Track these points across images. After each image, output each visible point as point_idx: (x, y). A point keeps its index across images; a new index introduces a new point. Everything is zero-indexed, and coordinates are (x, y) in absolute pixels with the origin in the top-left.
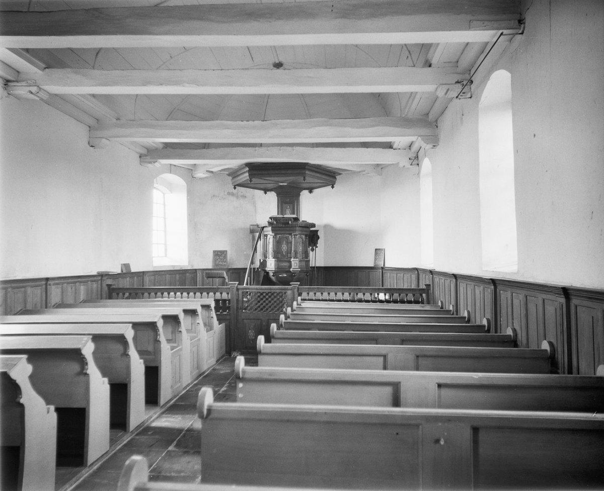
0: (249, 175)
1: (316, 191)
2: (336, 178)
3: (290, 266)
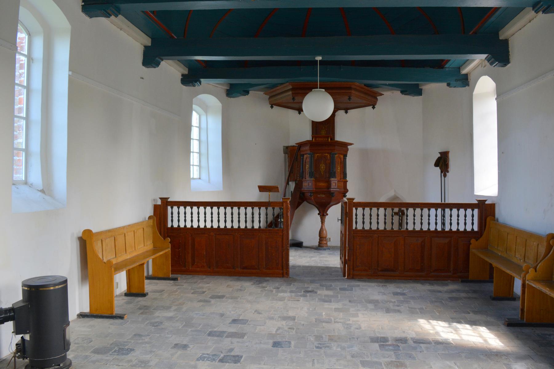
0: (292, 93)
1: (351, 112)
2: (377, 99)
3: (329, 186)
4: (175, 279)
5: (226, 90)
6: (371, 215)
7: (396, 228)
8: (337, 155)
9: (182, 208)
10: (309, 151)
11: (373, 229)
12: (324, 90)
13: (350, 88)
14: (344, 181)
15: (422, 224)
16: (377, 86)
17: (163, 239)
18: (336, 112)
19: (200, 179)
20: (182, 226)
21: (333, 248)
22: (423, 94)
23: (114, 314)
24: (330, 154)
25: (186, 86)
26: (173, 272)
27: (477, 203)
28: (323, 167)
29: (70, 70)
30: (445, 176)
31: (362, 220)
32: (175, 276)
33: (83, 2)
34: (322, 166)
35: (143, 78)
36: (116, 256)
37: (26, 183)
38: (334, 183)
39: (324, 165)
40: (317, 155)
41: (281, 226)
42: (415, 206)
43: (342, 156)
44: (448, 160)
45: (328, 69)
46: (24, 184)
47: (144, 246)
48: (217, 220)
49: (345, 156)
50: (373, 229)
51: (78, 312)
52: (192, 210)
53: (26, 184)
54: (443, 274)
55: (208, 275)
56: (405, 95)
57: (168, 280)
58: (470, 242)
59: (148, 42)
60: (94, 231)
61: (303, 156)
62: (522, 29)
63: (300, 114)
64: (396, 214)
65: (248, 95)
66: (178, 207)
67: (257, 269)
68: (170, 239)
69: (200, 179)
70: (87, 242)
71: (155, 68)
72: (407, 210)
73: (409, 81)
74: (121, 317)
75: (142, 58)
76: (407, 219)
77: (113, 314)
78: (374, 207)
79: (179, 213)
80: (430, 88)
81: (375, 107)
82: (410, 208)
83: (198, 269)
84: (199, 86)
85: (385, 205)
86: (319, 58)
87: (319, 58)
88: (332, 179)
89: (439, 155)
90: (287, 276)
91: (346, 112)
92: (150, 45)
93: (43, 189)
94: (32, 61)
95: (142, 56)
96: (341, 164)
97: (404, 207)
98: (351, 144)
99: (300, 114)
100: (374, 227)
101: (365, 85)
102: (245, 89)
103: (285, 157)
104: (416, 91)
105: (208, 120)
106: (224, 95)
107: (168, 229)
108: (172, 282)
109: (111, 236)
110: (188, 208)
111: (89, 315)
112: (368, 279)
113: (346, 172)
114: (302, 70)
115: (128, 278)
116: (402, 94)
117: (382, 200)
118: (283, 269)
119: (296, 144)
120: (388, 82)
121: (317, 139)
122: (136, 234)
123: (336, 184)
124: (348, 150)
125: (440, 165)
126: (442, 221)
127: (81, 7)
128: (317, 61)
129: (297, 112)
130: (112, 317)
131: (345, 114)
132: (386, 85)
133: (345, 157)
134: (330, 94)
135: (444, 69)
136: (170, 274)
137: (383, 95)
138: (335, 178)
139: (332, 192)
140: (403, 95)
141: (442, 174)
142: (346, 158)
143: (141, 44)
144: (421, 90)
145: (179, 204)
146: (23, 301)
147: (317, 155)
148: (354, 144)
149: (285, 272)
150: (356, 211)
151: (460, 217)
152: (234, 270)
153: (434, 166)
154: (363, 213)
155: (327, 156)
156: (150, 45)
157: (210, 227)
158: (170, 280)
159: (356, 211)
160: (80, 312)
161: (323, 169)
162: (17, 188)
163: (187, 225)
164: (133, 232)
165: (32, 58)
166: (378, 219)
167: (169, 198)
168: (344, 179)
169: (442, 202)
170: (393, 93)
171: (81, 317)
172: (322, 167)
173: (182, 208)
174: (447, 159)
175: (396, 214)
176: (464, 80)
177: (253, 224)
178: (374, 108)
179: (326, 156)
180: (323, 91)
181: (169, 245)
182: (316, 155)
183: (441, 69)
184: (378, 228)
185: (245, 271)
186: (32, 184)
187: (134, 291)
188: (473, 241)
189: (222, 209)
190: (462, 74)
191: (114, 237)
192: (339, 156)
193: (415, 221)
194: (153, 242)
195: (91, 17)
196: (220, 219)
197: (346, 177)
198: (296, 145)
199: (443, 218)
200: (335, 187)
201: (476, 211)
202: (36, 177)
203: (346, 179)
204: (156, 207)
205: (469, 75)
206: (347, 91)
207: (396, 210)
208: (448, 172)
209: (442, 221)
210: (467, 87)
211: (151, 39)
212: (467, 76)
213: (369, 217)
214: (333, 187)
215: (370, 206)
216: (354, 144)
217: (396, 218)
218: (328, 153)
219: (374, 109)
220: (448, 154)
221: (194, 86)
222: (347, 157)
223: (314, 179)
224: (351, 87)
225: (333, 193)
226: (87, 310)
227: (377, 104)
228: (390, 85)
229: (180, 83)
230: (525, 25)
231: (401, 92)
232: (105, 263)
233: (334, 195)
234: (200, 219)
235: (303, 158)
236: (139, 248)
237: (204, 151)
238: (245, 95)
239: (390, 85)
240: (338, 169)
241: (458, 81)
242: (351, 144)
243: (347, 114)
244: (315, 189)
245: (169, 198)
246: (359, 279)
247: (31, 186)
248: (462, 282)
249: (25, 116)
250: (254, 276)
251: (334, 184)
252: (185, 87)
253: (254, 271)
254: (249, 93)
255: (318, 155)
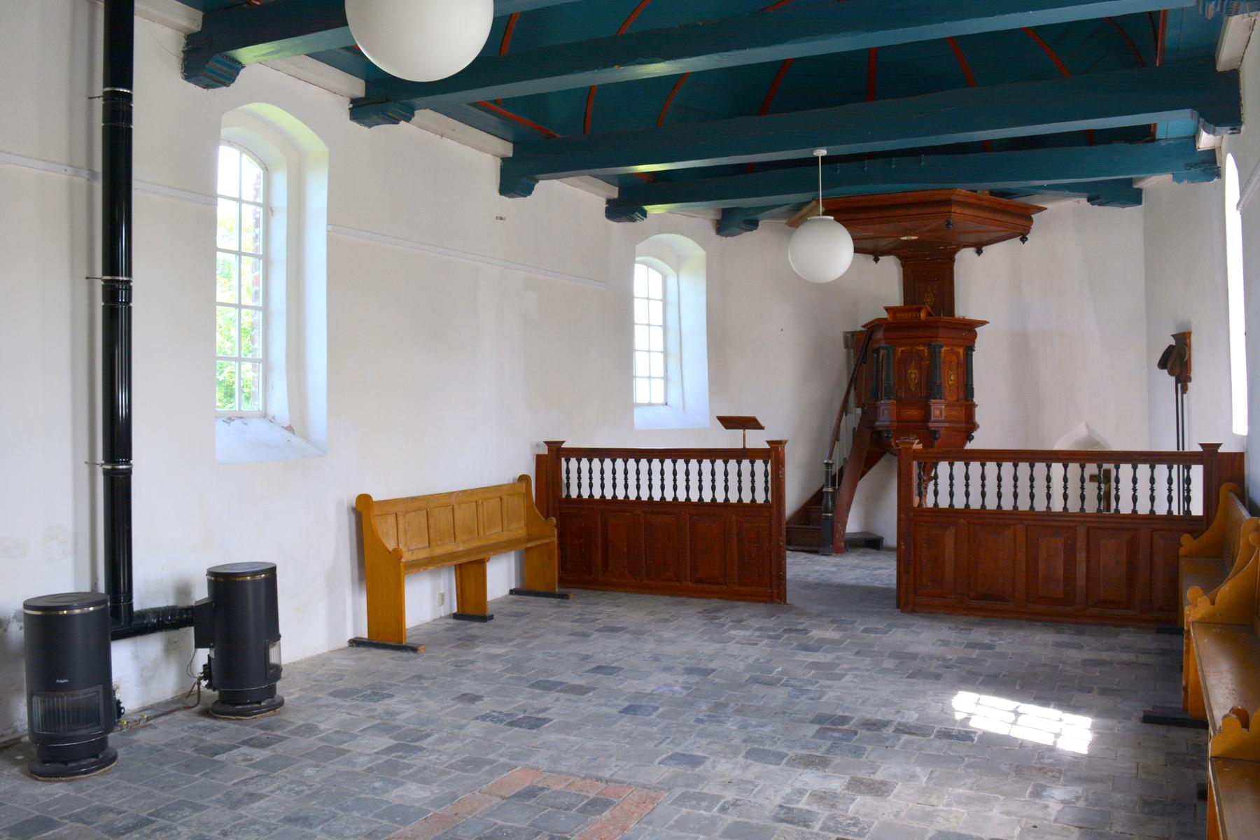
2: (1031, 220)
3: (927, 416)
4: (564, 596)
5: (715, 222)
6: (1032, 479)
7: (1091, 506)
8: (945, 348)
9: (694, 463)
10: (883, 342)
11: (1139, 513)
12: (832, 218)
13: (948, 202)
14: (966, 405)
15: (1152, 499)
16: (1029, 192)
17: (543, 519)
18: (956, 253)
19: (666, 404)
20: (682, 497)
21: (890, 549)
22: (1143, 202)
23: (404, 644)
24: (929, 345)
25: (618, 222)
26: (563, 582)
27: (1202, 450)
28: (913, 374)
29: (329, 224)
30: (1184, 390)
31: (1080, 492)
32: (564, 591)
33: (351, 103)
34: (911, 373)
35: (501, 218)
36: (429, 544)
37: (265, 416)
38: (938, 408)
39: (916, 371)
40: (902, 351)
41: (827, 504)
42: (1134, 458)
43: (961, 351)
44: (1187, 353)
45: (923, 164)
46: (262, 417)
47: (503, 531)
48: (763, 488)
49: (970, 349)
50: (1139, 513)
51: (351, 636)
52: (602, 465)
53: (265, 417)
54: (1116, 613)
55: (631, 592)
56: (1100, 205)
57: (552, 597)
58: (1179, 540)
59: (507, 149)
60: (376, 498)
61: (878, 353)
62: (1246, 52)
63: (876, 262)
64: (1093, 478)
65: (756, 229)
66: (737, 462)
67: (722, 584)
68: (556, 518)
69: (666, 404)
70: (364, 516)
71: (525, 196)
72: (1117, 468)
73: (1126, 175)
74: (413, 649)
75: (499, 181)
76: (1117, 489)
77: (401, 642)
78: (1142, 463)
79: (602, 472)
80: (1155, 183)
81: (1027, 239)
82: (1194, 464)
83: (614, 580)
84: (643, 220)
85: (1065, 457)
86: (821, 152)
87: (821, 152)
88: (932, 401)
89: (1173, 342)
90: (779, 601)
91: (979, 252)
92: (511, 155)
93: (290, 426)
94: (270, 212)
95: (499, 177)
96: (958, 367)
97: (1108, 462)
98: (983, 323)
99: (876, 262)
100: (959, 503)
101: (992, 193)
102: (749, 218)
103: (848, 355)
104: (1128, 195)
105: (681, 284)
106: (711, 231)
107: (561, 501)
108: (555, 601)
109: (420, 509)
110: (706, 464)
111: (366, 642)
112: (947, 614)
113: (972, 385)
114: (866, 170)
115: (459, 586)
116: (1092, 204)
117: (1061, 445)
118: (771, 588)
119: (863, 326)
120: (1045, 183)
121: (898, 315)
122: (480, 509)
123: (943, 412)
124: (975, 335)
125: (1169, 365)
126: (1186, 494)
127: (348, 112)
128: (818, 157)
129: (872, 257)
130: (401, 648)
131: (976, 255)
132: (1042, 187)
133: (969, 352)
134: (842, 224)
135: (1156, 143)
136: (557, 586)
137: (1046, 209)
138: (940, 398)
139: (932, 429)
140: (1096, 206)
141: (1179, 385)
142: (972, 355)
143: (494, 155)
144: (1140, 191)
145: (580, 453)
146: (951, 702)
147: (902, 351)
148: (988, 323)
149: (776, 592)
150: (568, 464)
151: (1156, 484)
152: (678, 584)
153: (1157, 366)
154: (1015, 474)
155: (924, 350)
156: (511, 155)
157: (947, 507)
158: (555, 597)
159: (568, 464)
160: (356, 636)
161: (915, 379)
162: (245, 424)
163: (743, 497)
164: (475, 504)
165: (271, 208)
166: (967, 485)
167: (563, 442)
168: (966, 400)
169: (1178, 449)
170: (1078, 202)
171: (354, 645)
172: (913, 376)
173: (694, 463)
174: (1187, 350)
175: (1093, 478)
176: (1207, 165)
177: (1049, 503)
178: (1024, 239)
179: (920, 350)
180: (830, 220)
181: (554, 530)
182: (900, 350)
183: (1149, 144)
184: (983, 506)
185: (700, 586)
186: (273, 417)
187: (469, 610)
188: (1186, 539)
189: (1007, 467)
190: (1198, 150)
191: (425, 511)
192: (952, 349)
193: (1085, 493)
194: (527, 525)
195: (370, 127)
196: (652, 483)
197: (972, 395)
198: (863, 329)
199: (1186, 486)
200: (941, 419)
201: (1197, 472)
202: (280, 405)
203: (972, 400)
204: (539, 459)
205: (1217, 151)
206: (942, 209)
207: (1092, 469)
208: (1189, 379)
209: (1186, 494)
210: (1215, 180)
211: (513, 143)
212: (1215, 152)
213: (1029, 483)
214: (935, 419)
215: (1081, 459)
216: (988, 323)
217: (1091, 489)
218: (924, 345)
219: (1026, 243)
220: (1190, 337)
221: (634, 220)
222: (974, 353)
223: (895, 402)
224: (950, 200)
225: (935, 431)
226: (364, 634)
227: (1032, 231)
228: (1050, 187)
229: (604, 216)
230: (1250, 37)
231: (1089, 201)
232: (390, 552)
233: (938, 436)
234: (954, 489)
235: (878, 356)
236: (488, 534)
237: (673, 348)
238: (752, 230)
239: (1050, 187)
240: (950, 379)
241: (1192, 166)
242: (983, 323)
243: (982, 255)
244: (896, 424)
245: (563, 442)
246: (926, 613)
247: (272, 420)
248: (1159, 631)
249: (261, 305)
250: (716, 598)
251: (937, 412)
252: (615, 224)
253: (716, 587)
254: (758, 226)
255: (903, 349)
